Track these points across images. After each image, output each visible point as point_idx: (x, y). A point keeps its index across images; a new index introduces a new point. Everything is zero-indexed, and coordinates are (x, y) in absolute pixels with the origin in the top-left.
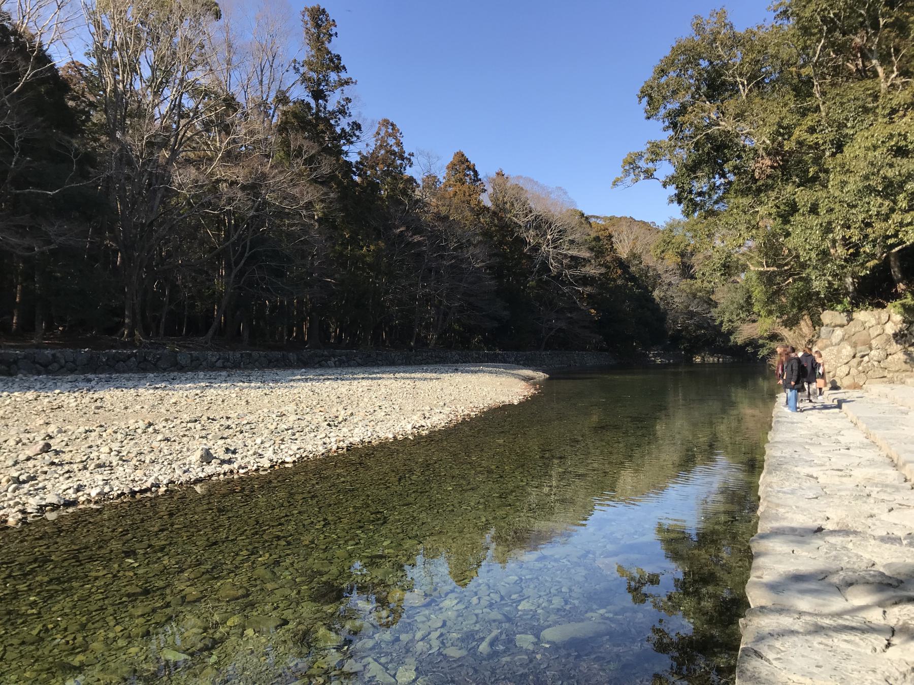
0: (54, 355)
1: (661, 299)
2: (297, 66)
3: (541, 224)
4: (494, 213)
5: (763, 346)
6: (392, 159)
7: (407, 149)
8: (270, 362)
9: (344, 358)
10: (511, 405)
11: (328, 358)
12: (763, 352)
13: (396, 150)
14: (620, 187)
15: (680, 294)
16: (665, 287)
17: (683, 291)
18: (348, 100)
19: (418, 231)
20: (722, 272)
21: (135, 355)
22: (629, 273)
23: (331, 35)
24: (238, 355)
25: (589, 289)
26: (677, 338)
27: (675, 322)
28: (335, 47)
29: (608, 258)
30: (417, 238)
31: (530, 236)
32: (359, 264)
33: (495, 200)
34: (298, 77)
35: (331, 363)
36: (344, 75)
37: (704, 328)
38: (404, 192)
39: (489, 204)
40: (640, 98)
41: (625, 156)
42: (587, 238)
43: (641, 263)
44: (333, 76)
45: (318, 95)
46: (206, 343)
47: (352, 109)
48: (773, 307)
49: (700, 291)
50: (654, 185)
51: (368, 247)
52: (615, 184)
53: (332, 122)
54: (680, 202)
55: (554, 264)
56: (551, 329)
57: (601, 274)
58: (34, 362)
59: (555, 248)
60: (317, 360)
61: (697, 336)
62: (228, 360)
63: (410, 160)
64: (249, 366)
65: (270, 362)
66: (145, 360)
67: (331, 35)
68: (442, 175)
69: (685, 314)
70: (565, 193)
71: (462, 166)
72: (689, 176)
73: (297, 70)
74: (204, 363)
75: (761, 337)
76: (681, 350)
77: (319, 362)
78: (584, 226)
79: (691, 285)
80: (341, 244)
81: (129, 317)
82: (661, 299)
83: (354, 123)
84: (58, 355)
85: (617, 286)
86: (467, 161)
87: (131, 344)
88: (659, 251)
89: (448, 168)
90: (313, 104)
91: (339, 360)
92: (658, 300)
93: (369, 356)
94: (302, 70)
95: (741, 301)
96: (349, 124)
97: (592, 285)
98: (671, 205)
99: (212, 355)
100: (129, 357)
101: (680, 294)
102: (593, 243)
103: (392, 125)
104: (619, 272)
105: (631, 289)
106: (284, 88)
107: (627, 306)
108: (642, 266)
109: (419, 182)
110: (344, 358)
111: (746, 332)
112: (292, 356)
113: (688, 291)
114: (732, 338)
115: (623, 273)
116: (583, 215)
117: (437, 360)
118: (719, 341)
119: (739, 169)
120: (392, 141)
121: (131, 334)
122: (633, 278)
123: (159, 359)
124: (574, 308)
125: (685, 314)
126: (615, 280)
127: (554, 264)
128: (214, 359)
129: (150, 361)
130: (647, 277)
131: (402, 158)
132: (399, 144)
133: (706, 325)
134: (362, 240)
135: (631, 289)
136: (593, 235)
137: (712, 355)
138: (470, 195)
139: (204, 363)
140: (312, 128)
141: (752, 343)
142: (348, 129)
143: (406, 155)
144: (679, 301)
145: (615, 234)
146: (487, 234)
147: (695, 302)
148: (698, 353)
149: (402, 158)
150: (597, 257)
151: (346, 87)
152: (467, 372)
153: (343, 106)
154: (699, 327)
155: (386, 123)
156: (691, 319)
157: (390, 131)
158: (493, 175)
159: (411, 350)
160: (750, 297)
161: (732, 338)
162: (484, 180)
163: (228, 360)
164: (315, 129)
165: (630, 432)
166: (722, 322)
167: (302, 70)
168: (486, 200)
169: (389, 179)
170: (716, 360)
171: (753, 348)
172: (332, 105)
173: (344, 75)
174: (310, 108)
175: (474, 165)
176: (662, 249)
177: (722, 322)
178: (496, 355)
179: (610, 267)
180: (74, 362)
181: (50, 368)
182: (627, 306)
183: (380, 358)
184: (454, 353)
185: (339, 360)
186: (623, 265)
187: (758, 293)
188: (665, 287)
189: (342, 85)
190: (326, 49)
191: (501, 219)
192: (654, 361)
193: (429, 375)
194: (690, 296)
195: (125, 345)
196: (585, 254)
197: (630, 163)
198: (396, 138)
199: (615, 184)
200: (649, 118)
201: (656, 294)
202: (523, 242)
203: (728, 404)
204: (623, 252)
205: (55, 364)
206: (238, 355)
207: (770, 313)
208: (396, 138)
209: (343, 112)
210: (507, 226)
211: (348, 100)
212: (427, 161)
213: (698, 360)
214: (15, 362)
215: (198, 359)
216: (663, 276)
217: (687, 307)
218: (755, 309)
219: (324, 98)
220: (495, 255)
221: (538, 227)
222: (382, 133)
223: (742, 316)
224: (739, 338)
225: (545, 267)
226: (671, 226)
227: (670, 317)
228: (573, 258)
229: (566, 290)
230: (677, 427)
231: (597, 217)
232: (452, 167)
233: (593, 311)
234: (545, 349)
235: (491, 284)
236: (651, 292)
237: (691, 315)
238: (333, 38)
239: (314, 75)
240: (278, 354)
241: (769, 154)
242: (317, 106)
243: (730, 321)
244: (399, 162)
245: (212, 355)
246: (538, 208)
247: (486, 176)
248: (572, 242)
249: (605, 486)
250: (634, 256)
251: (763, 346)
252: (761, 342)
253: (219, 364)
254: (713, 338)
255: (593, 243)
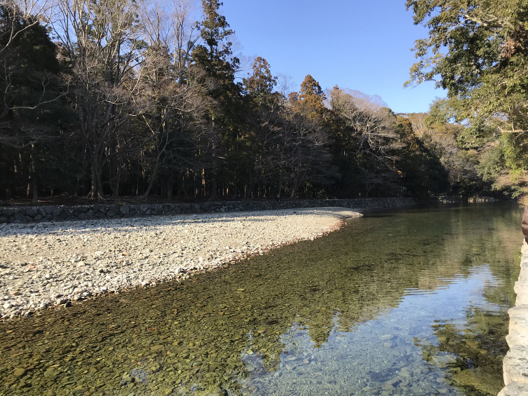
0: (38, 210)
1: (446, 163)
2: (199, 25)
3: (363, 118)
4: (332, 112)
5: (515, 190)
6: (263, 80)
7: (273, 74)
8: (182, 210)
9: (231, 206)
10: (308, 242)
11: (220, 207)
12: (515, 195)
13: (266, 75)
14: (409, 88)
15: (458, 159)
16: (448, 155)
17: (460, 157)
18: (230, 44)
19: (280, 124)
20: (478, 135)
21: (92, 209)
22: (423, 147)
23: (219, 4)
24: (161, 206)
25: (395, 158)
26: (457, 187)
27: (455, 177)
28: (221, 11)
29: (409, 138)
30: (276, 129)
31: (358, 126)
32: (236, 145)
33: (332, 103)
34: (199, 33)
35: (223, 210)
36: (227, 29)
37: (474, 180)
38: (271, 101)
39: (330, 108)
40: (408, 6)
41: (411, 66)
42: (394, 125)
43: (431, 140)
44: (221, 30)
45: (212, 42)
46: (144, 199)
47: (232, 48)
48: (521, 162)
49: (472, 157)
50: (432, 84)
51: (245, 135)
52: (406, 85)
53: (221, 58)
54: (445, 87)
55: (372, 142)
56: (372, 184)
57: (403, 148)
58: (25, 215)
59: (372, 132)
60: (213, 208)
61: (470, 186)
62: (154, 210)
63: (275, 81)
64: (168, 213)
65: (182, 210)
66: (99, 211)
67: (219, 4)
68: (298, 89)
69: (462, 172)
70: (380, 98)
71: (311, 84)
72: (450, 66)
73: (199, 28)
74: (138, 212)
75: (514, 185)
76: (460, 195)
77: (215, 209)
78: (392, 117)
79: (466, 154)
80: (228, 135)
81: (94, 185)
82: (446, 163)
83: (235, 58)
84: (41, 210)
85: (416, 156)
86: (314, 80)
87: (96, 201)
88: (429, 123)
89: (301, 86)
90: (208, 47)
91: (228, 208)
92: (443, 163)
93: (248, 205)
94: (202, 27)
95: (496, 159)
96: (232, 60)
97: (398, 155)
98: (438, 89)
99: (144, 207)
100: (88, 209)
101: (458, 159)
102: (399, 128)
103: (264, 60)
104: (417, 146)
105: (425, 157)
106: (192, 40)
107: (423, 168)
108: (432, 142)
109: (287, 96)
110: (231, 206)
111: (502, 182)
112: (197, 206)
113: (464, 157)
114: (493, 186)
115: (420, 147)
116: (390, 111)
117: (294, 205)
118: (485, 189)
119: (489, 54)
120: (263, 70)
121: (96, 195)
122: (426, 150)
123: (108, 211)
124: (387, 170)
125: (462, 172)
126: (414, 152)
127: (372, 142)
128: (145, 209)
129: (102, 212)
130: (435, 149)
131: (270, 80)
132: (268, 72)
133: (476, 178)
134: (241, 131)
135: (425, 157)
136: (398, 123)
137: (481, 197)
138: (315, 102)
139: (138, 212)
140: (213, 66)
141: (507, 188)
142: (231, 63)
143: (272, 78)
144: (457, 164)
145: (412, 122)
146: (327, 125)
147: (469, 163)
148: (471, 196)
149: (270, 80)
150: (401, 137)
151: (229, 36)
152: (307, 214)
153: (227, 48)
154: (471, 179)
155: (260, 59)
156: (466, 175)
157: (262, 64)
158: (331, 87)
159: (278, 200)
160: (503, 155)
161: (493, 186)
162: (325, 93)
163: (154, 210)
164: (210, 63)
165: (421, 253)
166: (482, 175)
167: (202, 27)
168: (327, 105)
169: (262, 94)
170: (483, 200)
171: (509, 192)
172: (220, 48)
173: (227, 29)
174: (205, 49)
175: (318, 83)
176: (431, 121)
177: (482, 175)
178: (334, 202)
179: (410, 144)
180: (51, 214)
181: (36, 218)
182: (423, 168)
183: (255, 205)
184: (305, 201)
185: (228, 208)
186: (419, 142)
187: (509, 151)
188: (448, 155)
189: (226, 35)
190: (215, 13)
191: (336, 116)
192: (442, 202)
193: (269, 217)
194: (465, 160)
195: (91, 202)
196: (391, 135)
197: (416, 71)
198: (266, 68)
199: (406, 85)
200: (416, 23)
201: (442, 160)
202: (352, 129)
203: (491, 230)
204: (419, 134)
205: (39, 215)
206: (161, 206)
207: (519, 166)
208: (266, 68)
209: (227, 51)
210: (340, 119)
211: (230, 44)
212: (288, 83)
213: (471, 201)
214: (13, 215)
215: (134, 209)
216: (447, 149)
217: (463, 167)
218: (507, 164)
219: (216, 44)
220: (333, 138)
221: (361, 120)
222: (257, 66)
223: (497, 169)
224: (497, 186)
225: (366, 143)
226: (437, 103)
227: (451, 174)
228: (385, 138)
229: (380, 158)
230: (457, 245)
231: (404, 114)
232: (304, 85)
233: (399, 171)
234: (369, 197)
235: (328, 156)
236: (439, 159)
237: (466, 172)
238: (220, 6)
239: (210, 30)
240: (188, 205)
241: (512, 37)
242: (211, 49)
243: (488, 173)
244: (268, 83)
245: (144, 207)
246: (361, 108)
247: (327, 90)
248: (384, 128)
249: (413, 284)
250: (427, 136)
251: (515, 190)
252: (513, 187)
253: (148, 212)
254: (482, 187)
255: (399, 128)
